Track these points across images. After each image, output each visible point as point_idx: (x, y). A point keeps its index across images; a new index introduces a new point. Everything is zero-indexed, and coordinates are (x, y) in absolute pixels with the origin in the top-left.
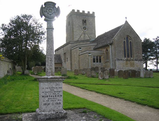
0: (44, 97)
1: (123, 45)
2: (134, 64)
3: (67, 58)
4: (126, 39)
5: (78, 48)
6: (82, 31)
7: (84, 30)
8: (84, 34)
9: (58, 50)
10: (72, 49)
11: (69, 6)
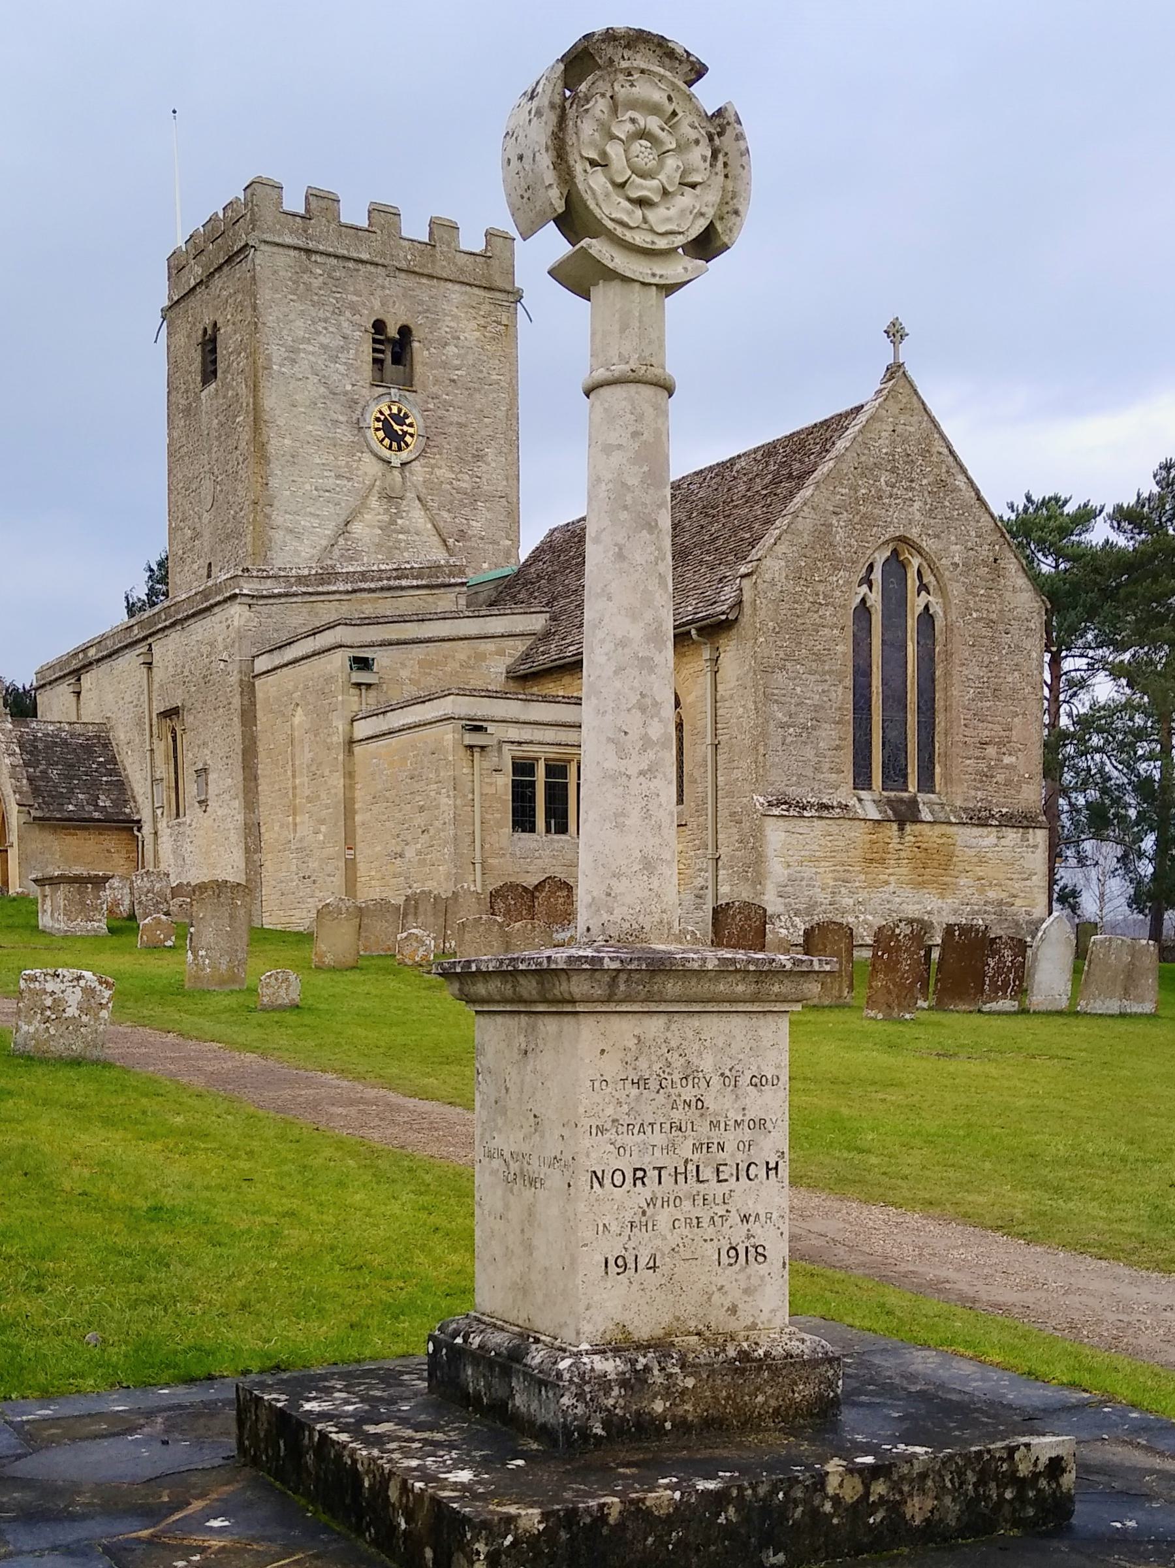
0: (607, 1181)
1: (844, 648)
2: (951, 856)
3: (202, 772)
4: (877, 576)
5: (340, 659)
6: (367, 458)
7: (386, 453)
8: (391, 498)
9: (87, 666)
10: (262, 664)
11: (174, 112)
